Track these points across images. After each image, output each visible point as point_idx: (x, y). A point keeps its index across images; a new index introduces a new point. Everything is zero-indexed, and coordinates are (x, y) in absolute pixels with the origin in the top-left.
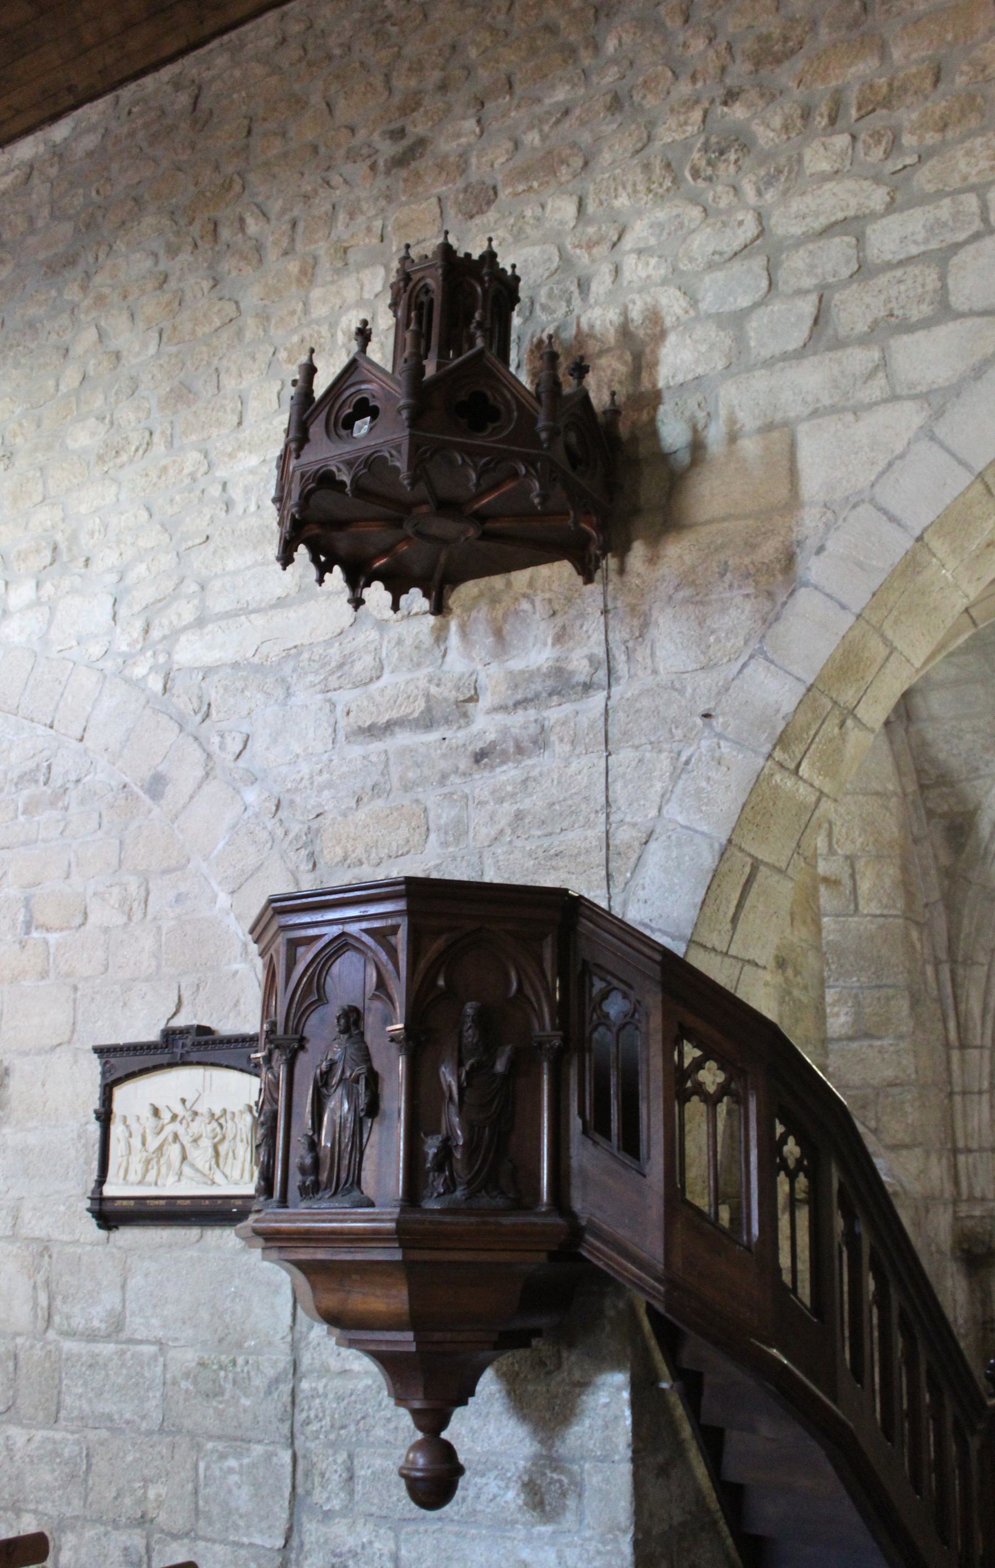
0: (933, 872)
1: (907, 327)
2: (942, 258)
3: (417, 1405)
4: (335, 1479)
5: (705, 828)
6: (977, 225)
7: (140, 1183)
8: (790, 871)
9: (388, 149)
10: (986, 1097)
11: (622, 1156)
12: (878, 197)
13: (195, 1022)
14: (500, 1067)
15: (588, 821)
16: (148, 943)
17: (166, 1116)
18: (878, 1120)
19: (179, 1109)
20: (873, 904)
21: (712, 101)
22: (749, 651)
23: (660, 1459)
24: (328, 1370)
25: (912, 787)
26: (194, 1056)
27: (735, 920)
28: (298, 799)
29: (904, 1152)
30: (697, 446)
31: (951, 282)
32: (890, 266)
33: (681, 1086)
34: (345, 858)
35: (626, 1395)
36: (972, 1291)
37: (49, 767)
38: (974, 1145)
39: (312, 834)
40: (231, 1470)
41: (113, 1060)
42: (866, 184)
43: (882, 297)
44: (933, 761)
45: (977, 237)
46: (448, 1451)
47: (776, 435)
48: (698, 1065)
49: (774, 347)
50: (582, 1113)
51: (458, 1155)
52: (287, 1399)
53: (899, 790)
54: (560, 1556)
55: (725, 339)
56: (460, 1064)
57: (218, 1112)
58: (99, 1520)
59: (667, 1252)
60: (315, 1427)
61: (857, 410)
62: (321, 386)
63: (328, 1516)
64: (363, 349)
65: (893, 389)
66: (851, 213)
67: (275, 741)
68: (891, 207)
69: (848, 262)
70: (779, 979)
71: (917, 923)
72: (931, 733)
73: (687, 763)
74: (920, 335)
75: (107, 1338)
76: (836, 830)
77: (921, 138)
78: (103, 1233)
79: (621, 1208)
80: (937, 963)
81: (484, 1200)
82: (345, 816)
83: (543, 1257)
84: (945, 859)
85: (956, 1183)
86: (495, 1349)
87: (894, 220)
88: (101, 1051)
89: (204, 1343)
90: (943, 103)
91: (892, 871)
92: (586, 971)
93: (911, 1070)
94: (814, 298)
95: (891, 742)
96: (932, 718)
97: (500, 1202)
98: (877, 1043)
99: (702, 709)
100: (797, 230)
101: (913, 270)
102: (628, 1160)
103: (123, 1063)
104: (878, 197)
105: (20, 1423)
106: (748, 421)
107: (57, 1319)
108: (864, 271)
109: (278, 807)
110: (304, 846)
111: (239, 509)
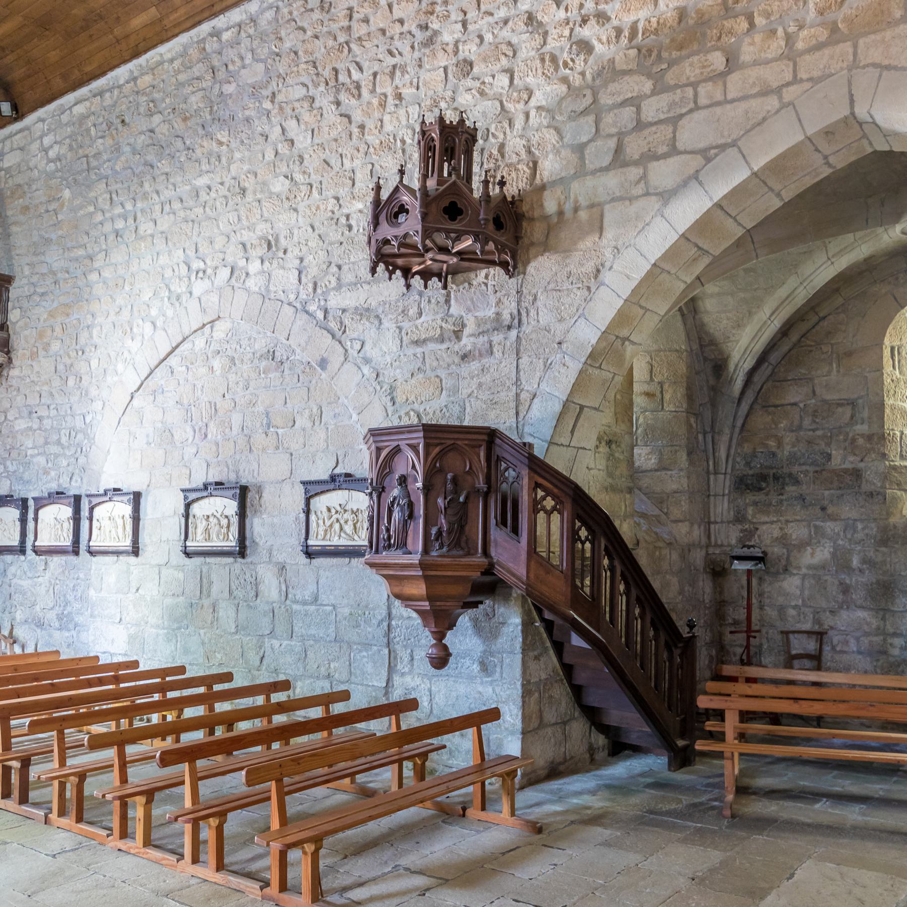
0: (705, 388)
1: (657, 158)
2: (675, 121)
3: (433, 630)
4: (406, 659)
5: (557, 394)
6: (692, 105)
7: (323, 539)
8: (601, 408)
9: (420, 36)
10: (726, 498)
11: (512, 534)
12: (648, 86)
13: (344, 471)
14: (461, 499)
15: (509, 387)
16: (322, 435)
17: (333, 511)
18: (668, 509)
19: (339, 508)
20: (671, 406)
21: (575, 24)
22: (578, 314)
23: (536, 653)
24: (403, 617)
25: (695, 347)
26: (344, 486)
27: (572, 432)
28: (386, 372)
29: (680, 524)
30: (561, 213)
31: (677, 134)
32: (652, 124)
33: (536, 507)
34: (407, 400)
35: (520, 627)
36: (715, 588)
37: (274, 352)
38: (719, 520)
39: (392, 389)
40: (364, 657)
41: (309, 487)
42: (643, 78)
43: (646, 141)
44: (707, 333)
45: (691, 111)
46: (445, 648)
47: (595, 209)
48: (544, 498)
49: (597, 165)
50: (496, 517)
51: (444, 534)
52: (386, 628)
53: (689, 350)
54: (494, 690)
55: (574, 158)
56: (445, 498)
57: (355, 510)
58: (311, 677)
59: (528, 572)
60: (398, 639)
61: (631, 199)
62: (385, 195)
63: (403, 674)
64: (402, 178)
65: (647, 189)
66: (635, 94)
67: (375, 345)
68: (654, 93)
69: (632, 120)
70: (607, 449)
71: (695, 414)
72: (707, 319)
73: (551, 364)
74: (661, 161)
75: (311, 604)
76: (654, 369)
77: (670, 54)
78: (308, 560)
79: (509, 555)
80: (705, 434)
81: (454, 552)
82: (406, 381)
83: (479, 573)
84: (712, 382)
85: (709, 537)
86: (462, 608)
87: (654, 99)
88: (304, 483)
89: (352, 606)
90: (682, 35)
91: (681, 391)
92: (499, 459)
93: (685, 485)
94: (615, 139)
95: (685, 324)
96: (707, 312)
97: (461, 553)
98: (669, 473)
99: (557, 340)
100: (610, 102)
101: (662, 127)
102: (514, 536)
103: (312, 489)
104: (648, 86)
105: (277, 639)
106: (583, 202)
107: (290, 596)
108: (640, 125)
109: (377, 376)
110: (389, 394)
111: (355, 229)
